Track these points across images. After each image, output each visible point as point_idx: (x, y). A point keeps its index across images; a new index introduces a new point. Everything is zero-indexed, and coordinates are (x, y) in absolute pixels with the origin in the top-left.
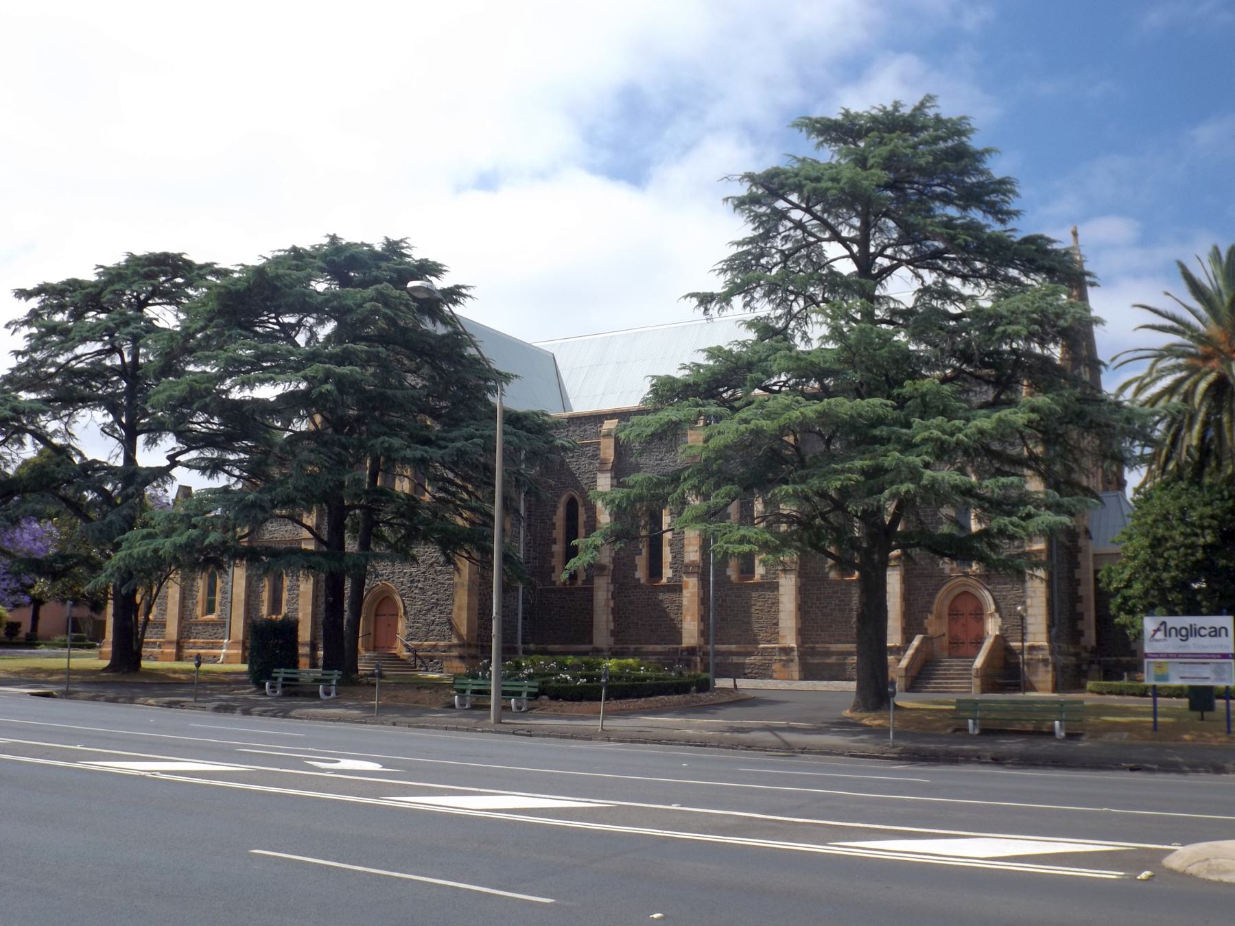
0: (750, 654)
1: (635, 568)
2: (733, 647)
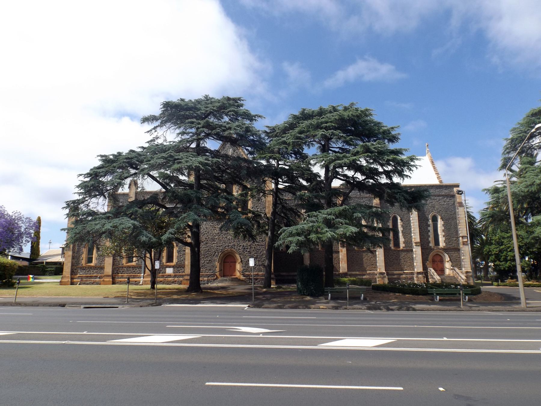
0: (364, 275)
1: (429, 242)
2: (357, 273)
